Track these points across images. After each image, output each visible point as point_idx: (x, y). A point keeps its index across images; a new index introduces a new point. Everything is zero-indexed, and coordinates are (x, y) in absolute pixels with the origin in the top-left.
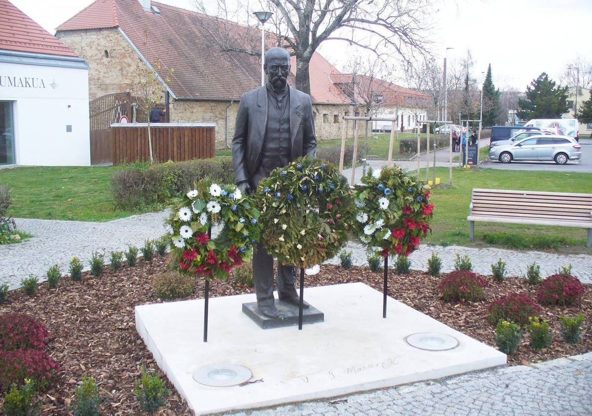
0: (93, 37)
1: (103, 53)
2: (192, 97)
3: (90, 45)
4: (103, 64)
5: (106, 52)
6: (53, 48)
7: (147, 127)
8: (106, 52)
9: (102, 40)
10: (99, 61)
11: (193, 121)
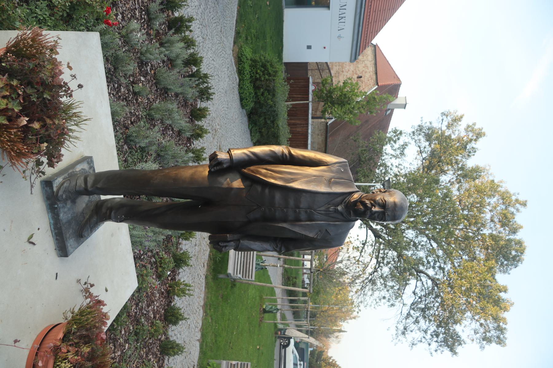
0: (371, 69)
1: (360, 75)
2: (329, 135)
3: (366, 66)
4: (353, 75)
5: (361, 77)
6: (365, 38)
7: (308, 100)
8: (361, 77)
9: (369, 74)
10: (355, 72)
11: (312, 135)
